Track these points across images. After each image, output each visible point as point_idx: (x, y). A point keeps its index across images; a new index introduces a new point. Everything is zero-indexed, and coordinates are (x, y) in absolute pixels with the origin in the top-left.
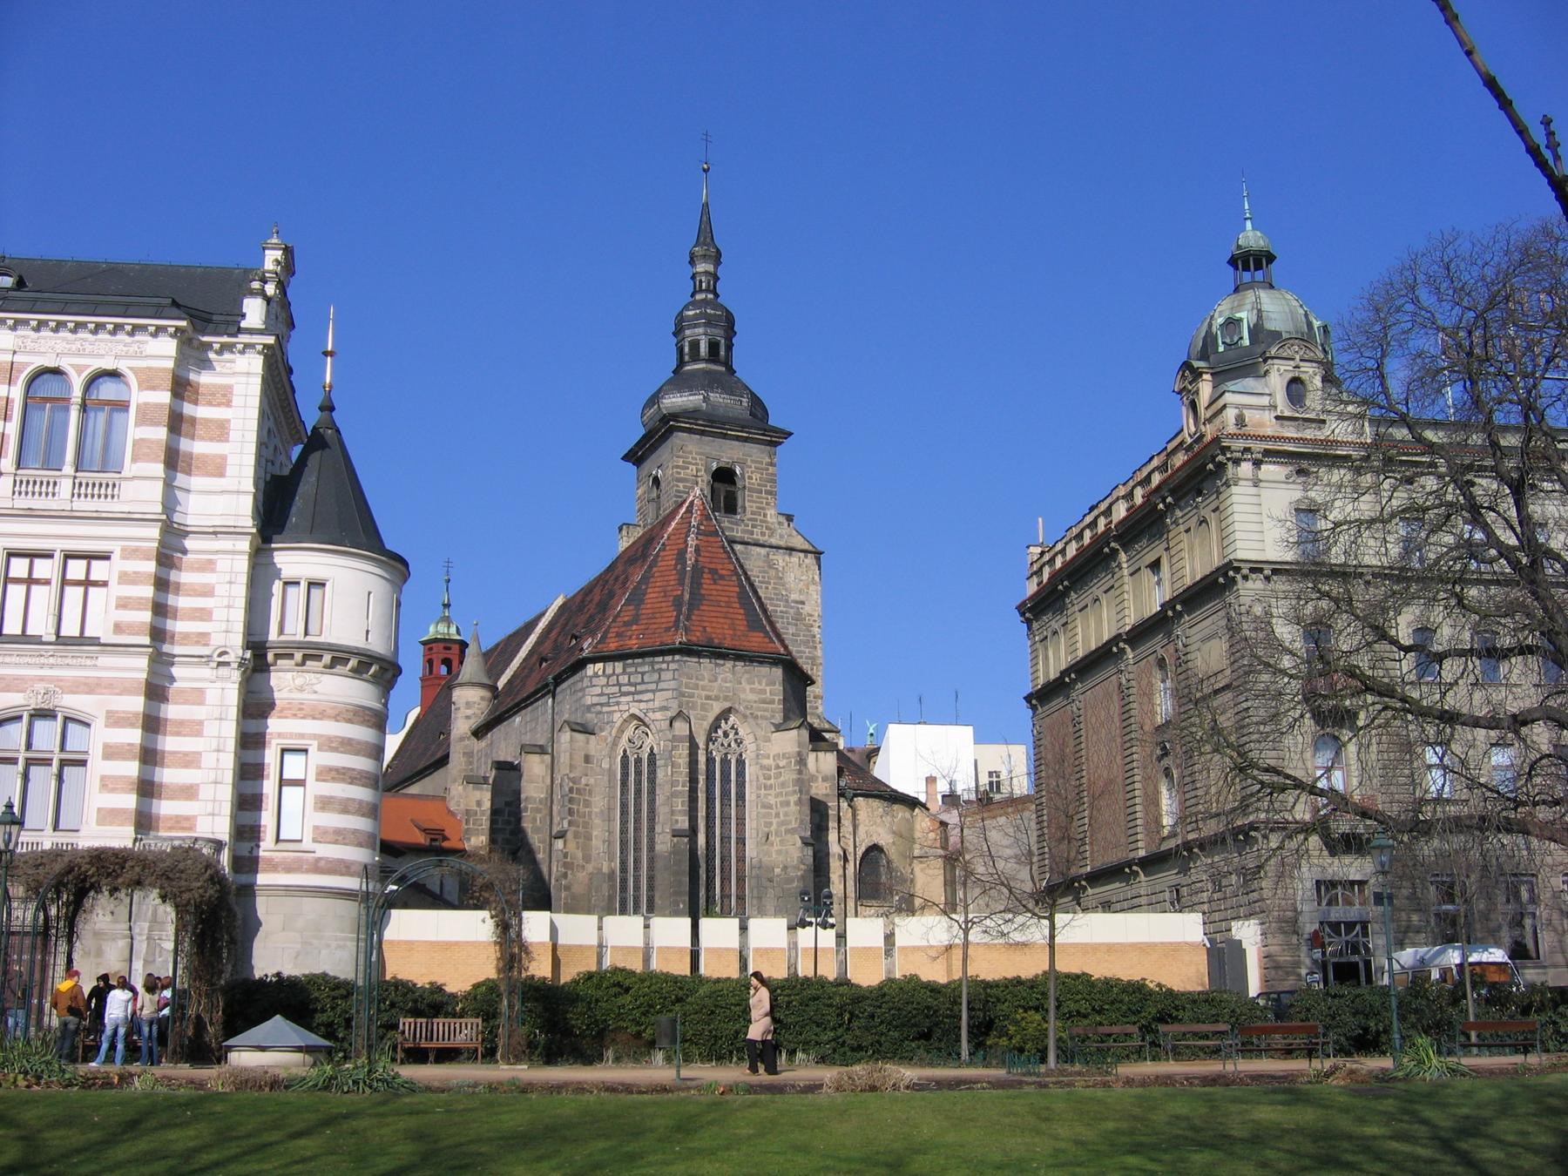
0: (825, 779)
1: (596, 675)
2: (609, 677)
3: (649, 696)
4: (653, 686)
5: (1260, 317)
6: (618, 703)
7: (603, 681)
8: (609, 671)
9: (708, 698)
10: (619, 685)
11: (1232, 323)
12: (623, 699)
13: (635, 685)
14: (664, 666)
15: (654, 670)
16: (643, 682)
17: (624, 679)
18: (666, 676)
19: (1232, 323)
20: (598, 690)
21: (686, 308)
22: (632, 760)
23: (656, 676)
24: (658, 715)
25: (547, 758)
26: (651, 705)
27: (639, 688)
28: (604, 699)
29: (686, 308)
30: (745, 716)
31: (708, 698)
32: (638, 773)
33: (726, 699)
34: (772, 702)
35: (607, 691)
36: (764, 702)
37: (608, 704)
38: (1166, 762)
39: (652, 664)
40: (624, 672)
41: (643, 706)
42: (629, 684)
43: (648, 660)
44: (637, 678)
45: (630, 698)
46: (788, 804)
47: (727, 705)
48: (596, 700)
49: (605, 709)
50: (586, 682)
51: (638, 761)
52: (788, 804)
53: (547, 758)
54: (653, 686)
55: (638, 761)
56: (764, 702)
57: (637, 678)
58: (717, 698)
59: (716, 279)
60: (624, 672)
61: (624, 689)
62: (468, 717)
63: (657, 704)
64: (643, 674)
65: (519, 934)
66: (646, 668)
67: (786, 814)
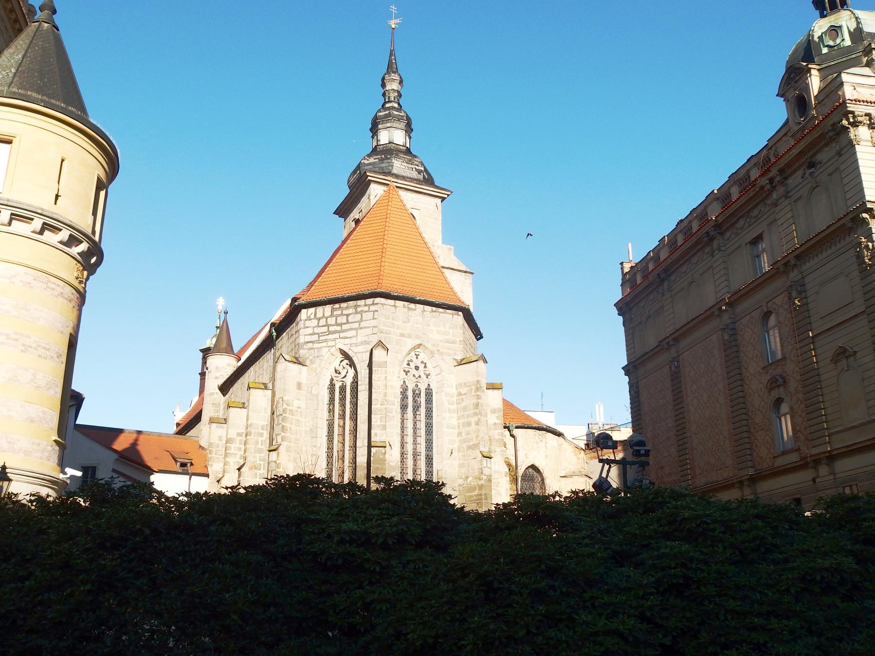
0: (494, 411)
1: (309, 319)
2: (319, 319)
3: (353, 333)
4: (356, 325)
5: (858, 23)
6: (326, 341)
7: (315, 322)
8: (319, 315)
9: (402, 335)
10: (328, 326)
11: (835, 30)
12: (331, 337)
13: (341, 325)
14: (366, 308)
15: (357, 313)
16: (348, 322)
17: (331, 321)
18: (367, 316)
19: (835, 30)
20: (310, 331)
21: (379, 111)
22: (338, 385)
23: (358, 317)
24: (360, 349)
25: (269, 393)
26: (354, 341)
27: (344, 327)
28: (315, 338)
29: (379, 111)
30: (432, 353)
31: (402, 335)
32: (343, 399)
33: (417, 337)
34: (454, 342)
35: (317, 330)
36: (448, 342)
37: (319, 342)
38: (779, 392)
39: (356, 306)
40: (332, 315)
41: (347, 341)
42: (337, 324)
43: (351, 303)
44: (343, 319)
45: (336, 336)
46: (469, 424)
47: (418, 342)
48: (308, 339)
49: (316, 345)
50: (301, 325)
51: (343, 389)
52: (469, 424)
53: (269, 393)
54: (356, 325)
55: (343, 389)
56: (448, 342)
57: (343, 319)
58: (410, 336)
59: (400, 95)
60: (332, 315)
61: (331, 328)
62: (216, 378)
63: (359, 339)
64: (348, 315)
65: (167, 498)
66: (351, 311)
67: (468, 434)
